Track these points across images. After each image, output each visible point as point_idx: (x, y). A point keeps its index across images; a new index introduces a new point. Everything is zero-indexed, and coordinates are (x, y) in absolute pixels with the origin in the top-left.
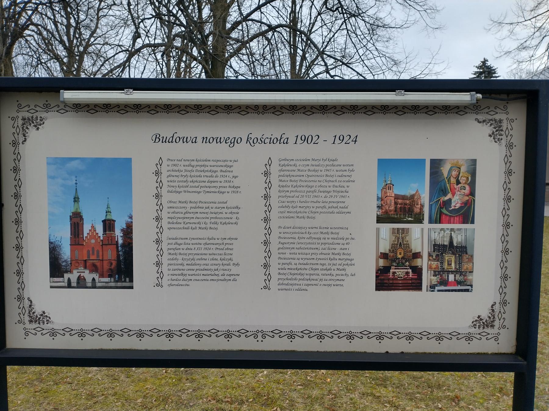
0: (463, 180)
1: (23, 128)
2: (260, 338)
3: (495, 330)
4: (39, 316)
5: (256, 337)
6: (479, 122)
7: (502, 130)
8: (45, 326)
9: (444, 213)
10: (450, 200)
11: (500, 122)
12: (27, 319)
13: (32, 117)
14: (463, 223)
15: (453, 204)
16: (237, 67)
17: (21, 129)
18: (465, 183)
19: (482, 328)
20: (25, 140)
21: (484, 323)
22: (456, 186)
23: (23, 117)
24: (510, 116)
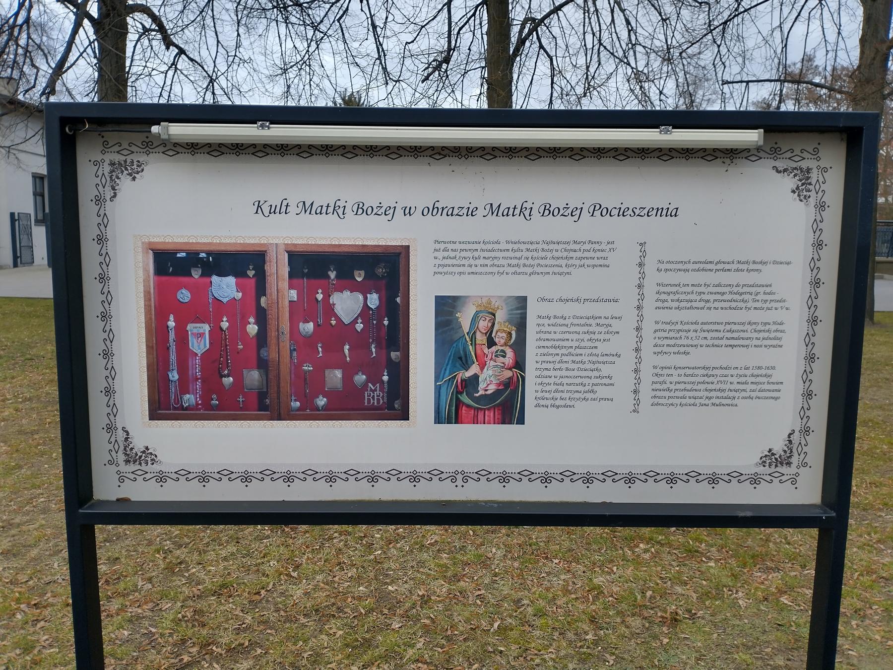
0: (500, 338)
1: (111, 177)
2: (459, 482)
3: (793, 470)
4: (140, 454)
5: (454, 480)
6: (778, 172)
7: (810, 184)
8: (150, 468)
9: (464, 404)
10: (476, 377)
11: (808, 172)
12: (121, 457)
13: (125, 161)
14: (503, 423)
15: (482, 386)
16: (532, 90)
17: (108, 179)
18: (505, 344)
19: (773, 466)
20: (115, 196)
21: (776, 460)
22: (486, 350)
23: (111, 161)
24: (822, 164)
